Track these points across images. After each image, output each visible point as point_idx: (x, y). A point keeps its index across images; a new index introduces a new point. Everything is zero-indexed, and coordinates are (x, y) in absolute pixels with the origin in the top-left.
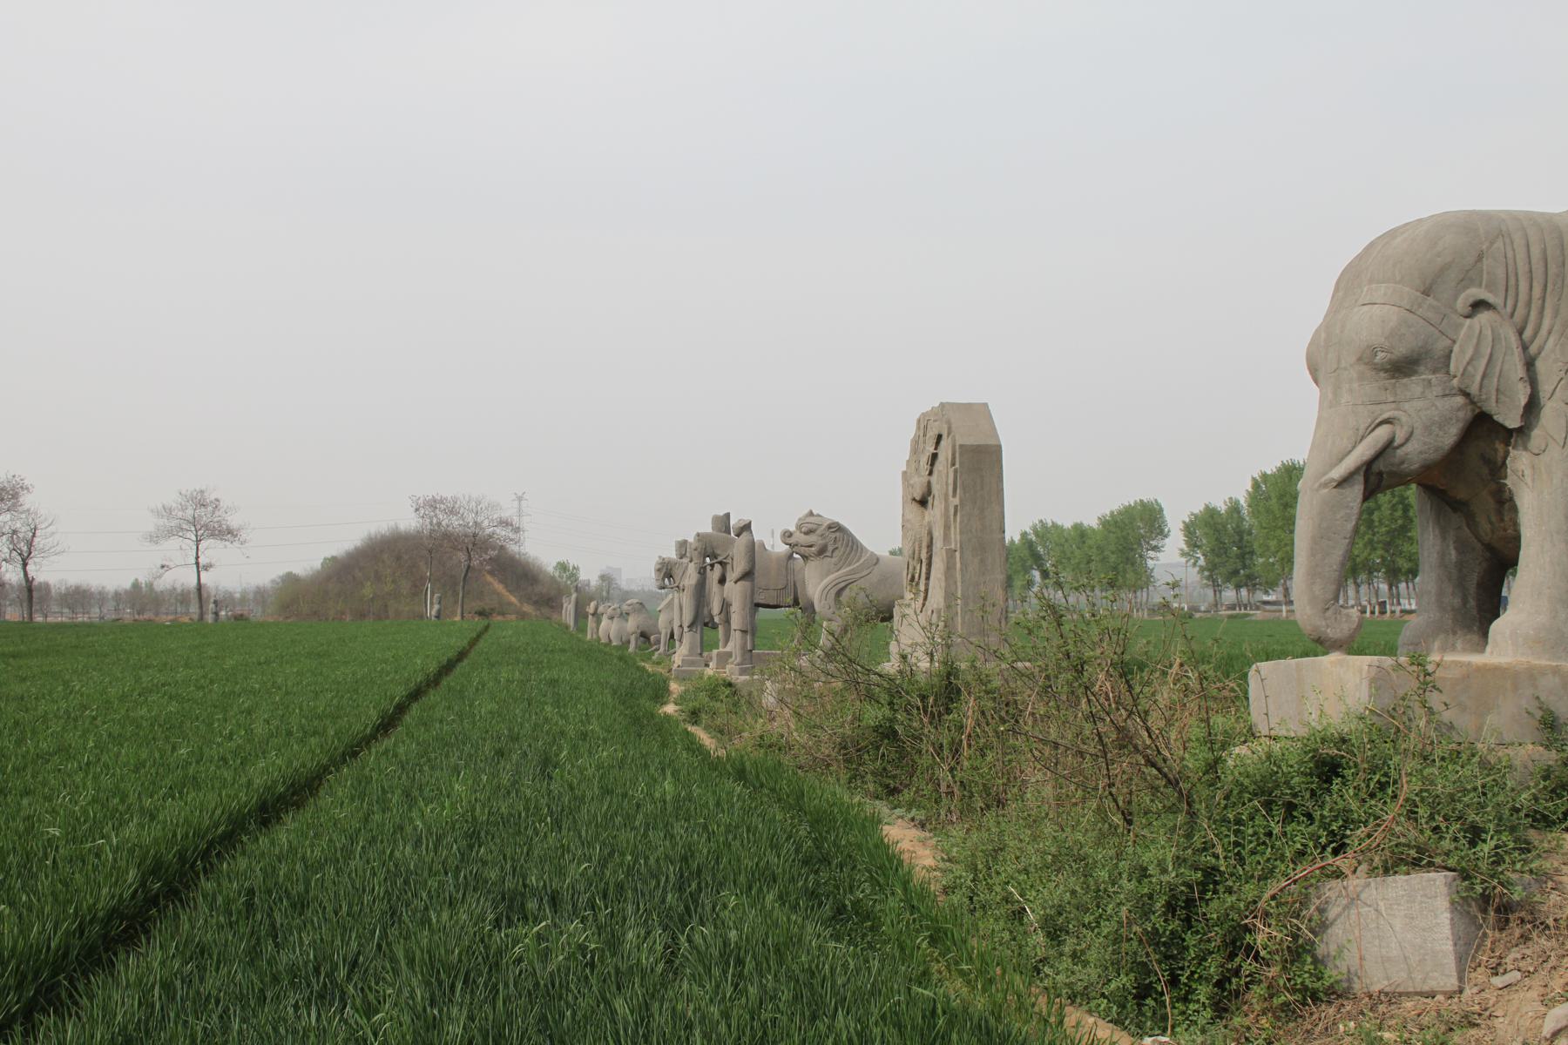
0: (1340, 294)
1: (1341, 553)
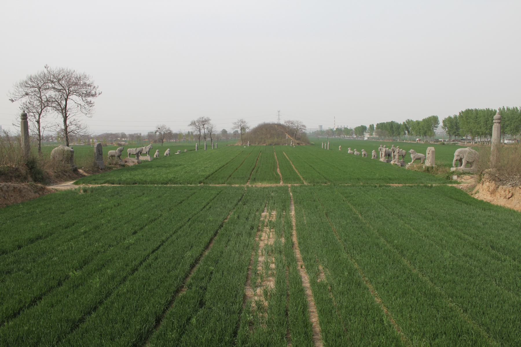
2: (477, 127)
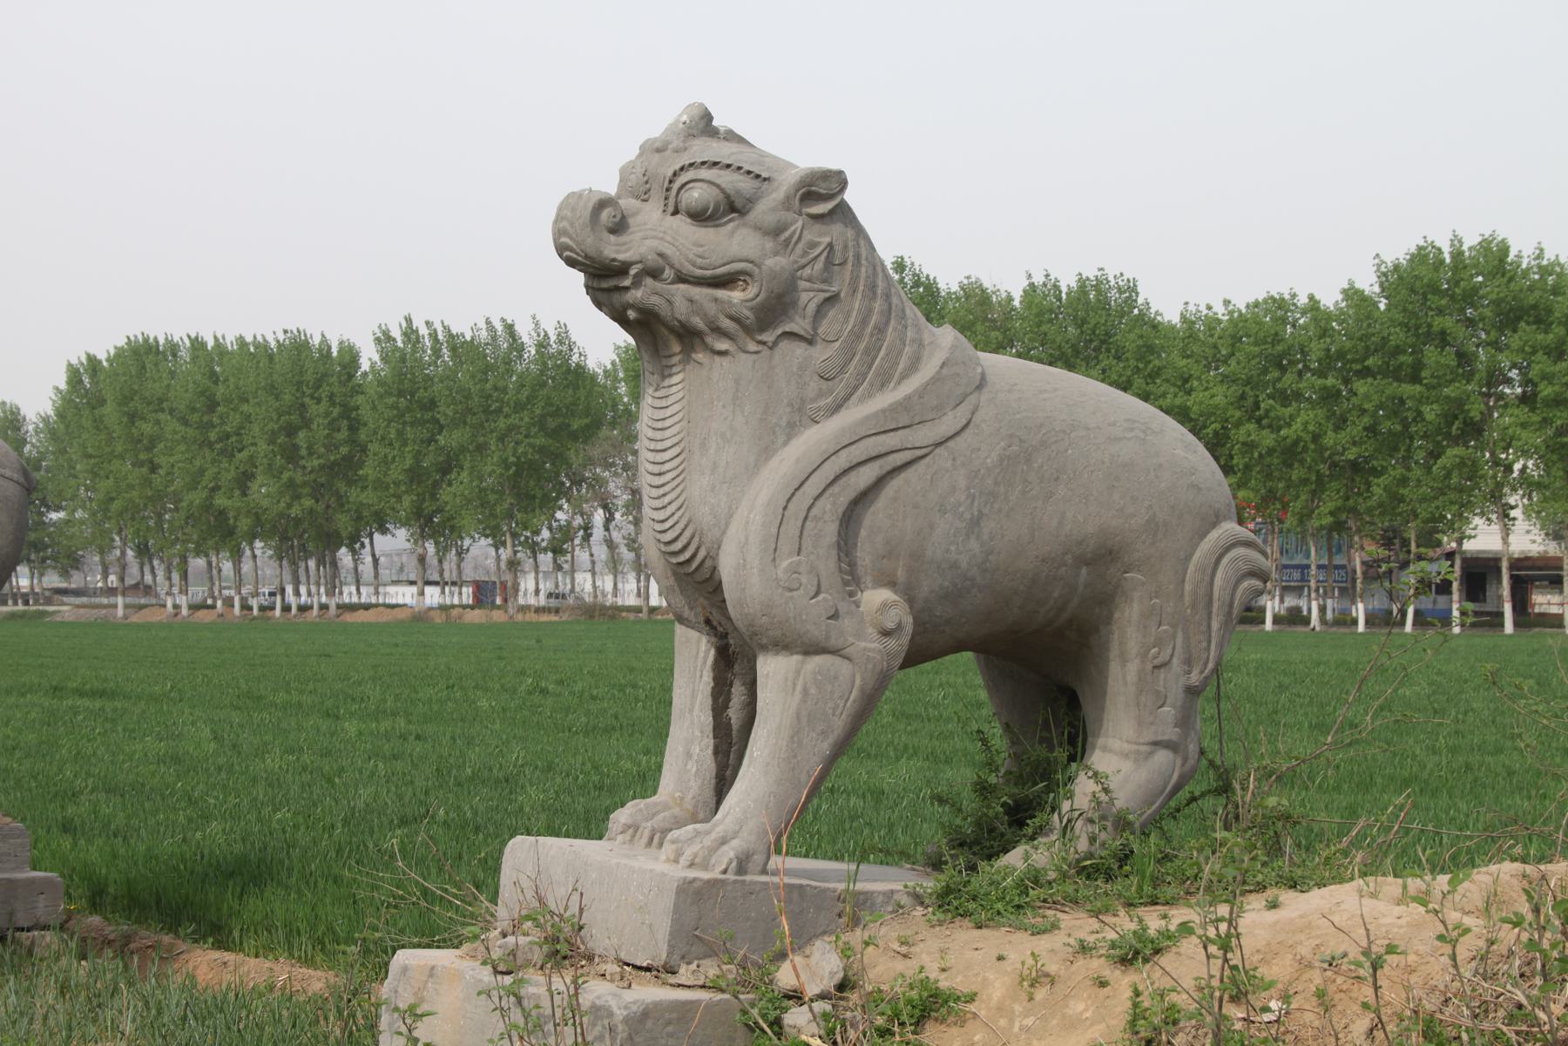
2: (216, 478)
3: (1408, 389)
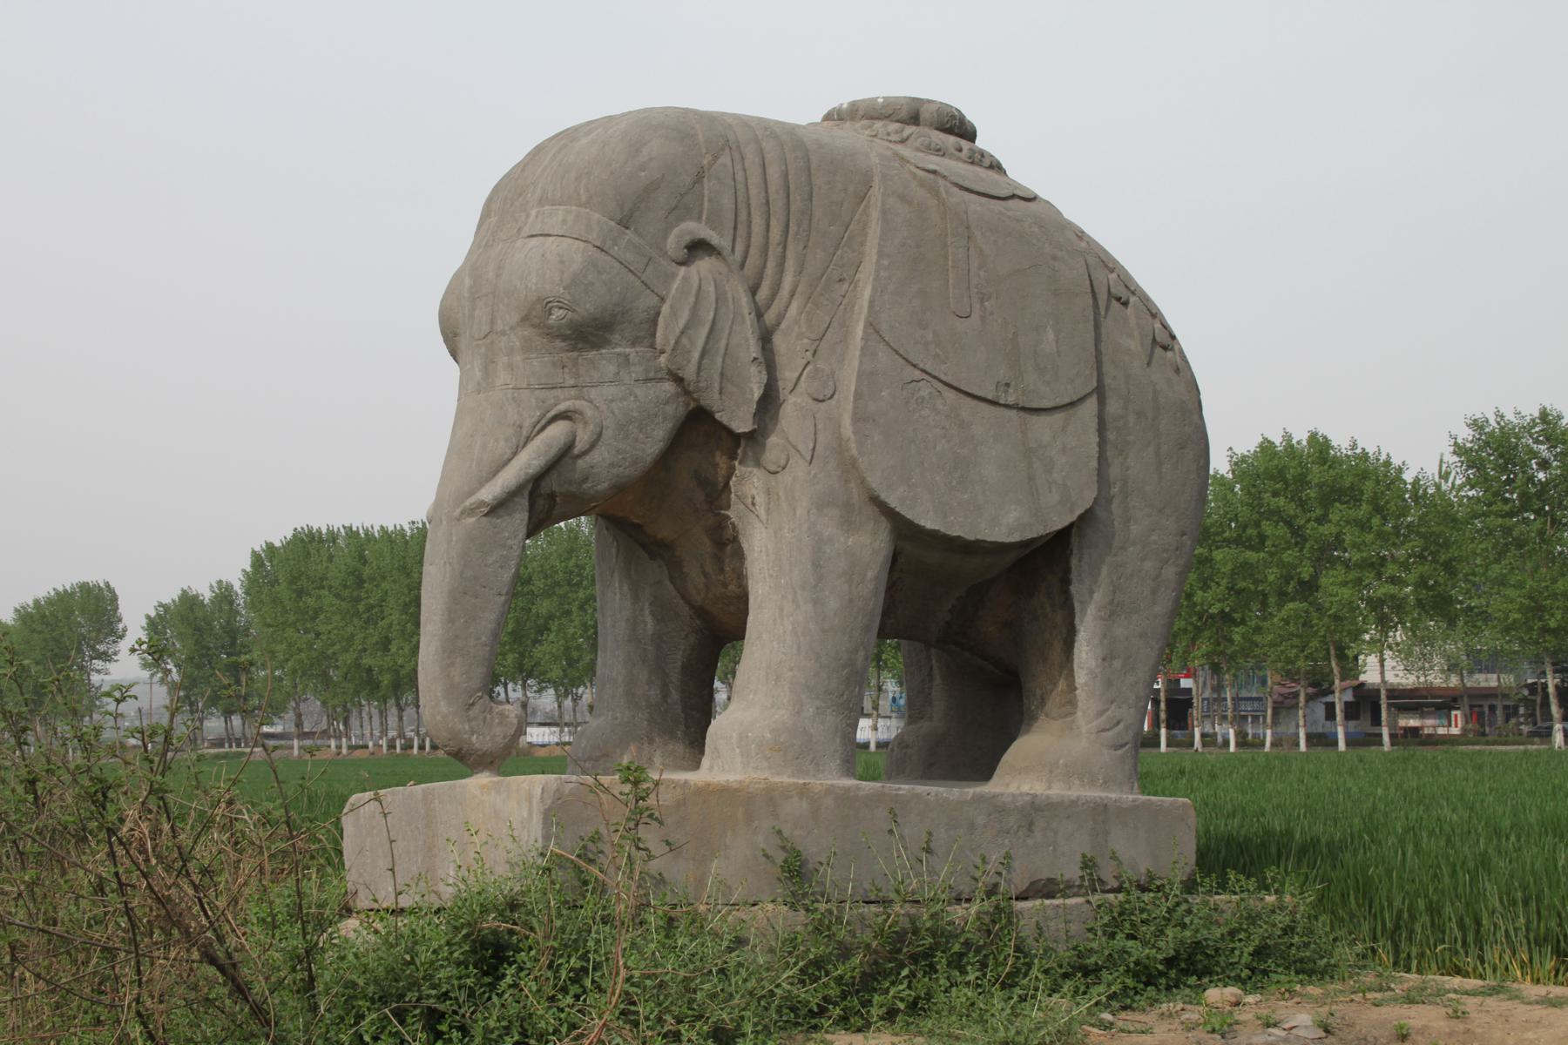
0: (494, 219)
1: (493, 617)
3: (1251, 556)
